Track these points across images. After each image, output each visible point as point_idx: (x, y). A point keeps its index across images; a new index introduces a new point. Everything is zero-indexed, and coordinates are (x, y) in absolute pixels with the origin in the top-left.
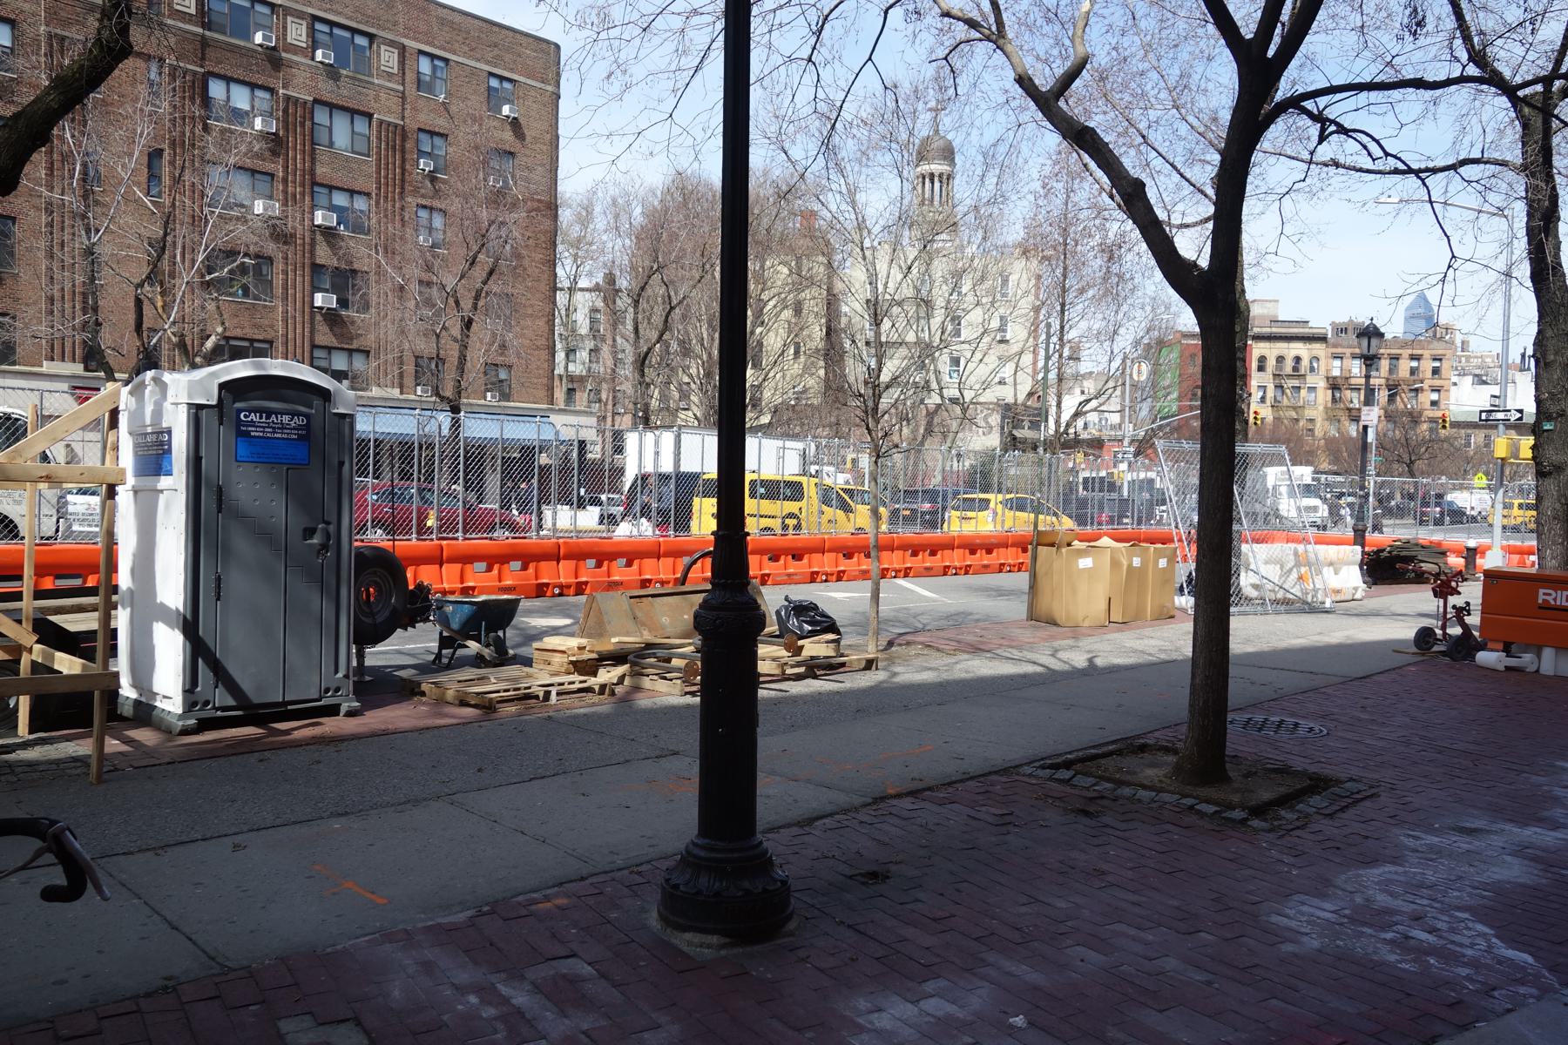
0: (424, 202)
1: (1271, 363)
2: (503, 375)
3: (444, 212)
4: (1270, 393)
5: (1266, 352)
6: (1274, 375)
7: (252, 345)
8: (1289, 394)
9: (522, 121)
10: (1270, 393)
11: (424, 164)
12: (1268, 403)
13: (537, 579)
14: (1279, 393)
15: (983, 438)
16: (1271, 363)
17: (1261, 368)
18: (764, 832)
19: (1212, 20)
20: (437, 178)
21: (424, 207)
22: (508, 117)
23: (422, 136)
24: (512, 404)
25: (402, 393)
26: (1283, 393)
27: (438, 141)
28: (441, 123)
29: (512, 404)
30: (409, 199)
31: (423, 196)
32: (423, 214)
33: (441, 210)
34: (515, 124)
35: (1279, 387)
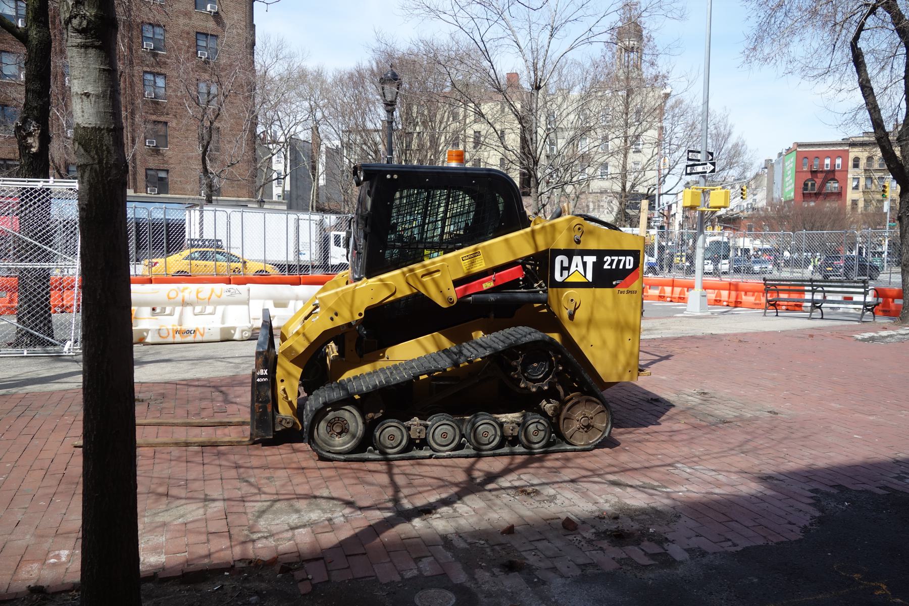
0: (148, 70)
1: (863, 163)
2: (162, 175)
3: (165, 76)
4: (862, 182)
5: (860, 155)
6: (865, 170)
7: (5, 162)
8: (877, 183)
9: (222, 14)
10: (862, 182)
11: (149, 45)
12: (861, 189)
13: (533, 232)
14: (869, 183)
15: (607, 215)
16: (863, 163)
17: (856, 166)
18: (557, 291)
19: (533, 330)
20: (158, 54)
21: (150, 73)
22: (211, 12)
23: (146, 27)
24: (169, 196)
25: (135, 192)
26: (872, 182)
27: (158, 30)
28: (160, 18)
29: (169, 196)
30: (136, 68)
31: (147, 66)
32: (149, 77)
33: (162, 74)
34: (217, 16)
35: (869, 178)
